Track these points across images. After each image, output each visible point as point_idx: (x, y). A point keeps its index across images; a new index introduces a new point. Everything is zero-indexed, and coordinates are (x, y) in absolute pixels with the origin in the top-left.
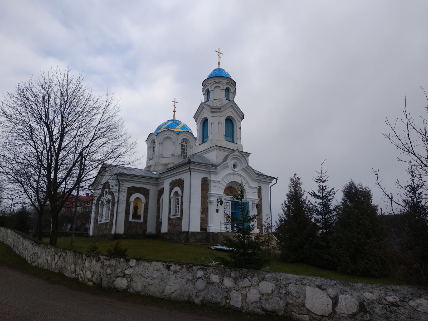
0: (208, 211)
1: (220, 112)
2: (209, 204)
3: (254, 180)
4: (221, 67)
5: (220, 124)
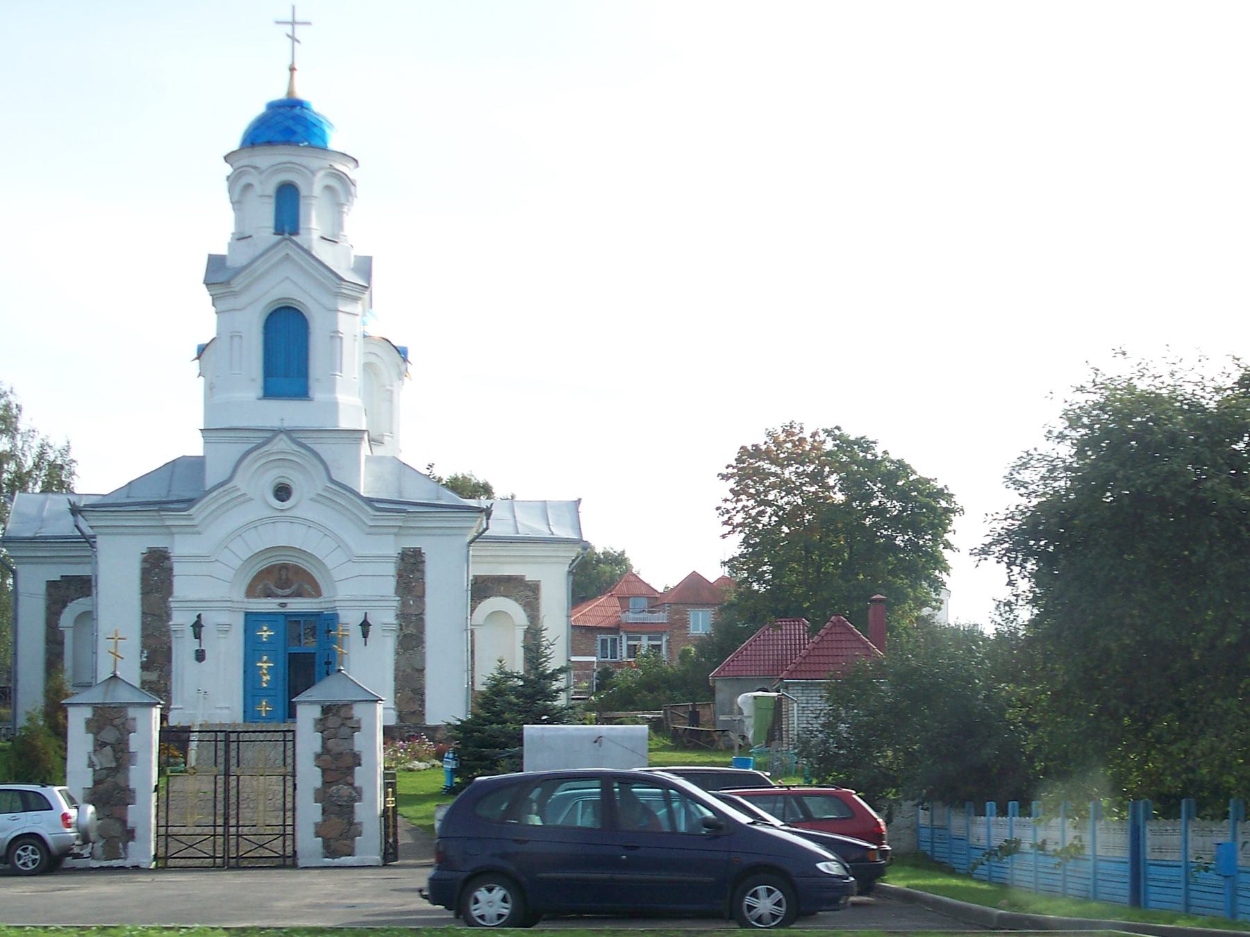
0: (170, 661)
1: (235, 294)
2: (173, 635)
3: (374, 531)
4: (300, 94)
5: (236, 340)
